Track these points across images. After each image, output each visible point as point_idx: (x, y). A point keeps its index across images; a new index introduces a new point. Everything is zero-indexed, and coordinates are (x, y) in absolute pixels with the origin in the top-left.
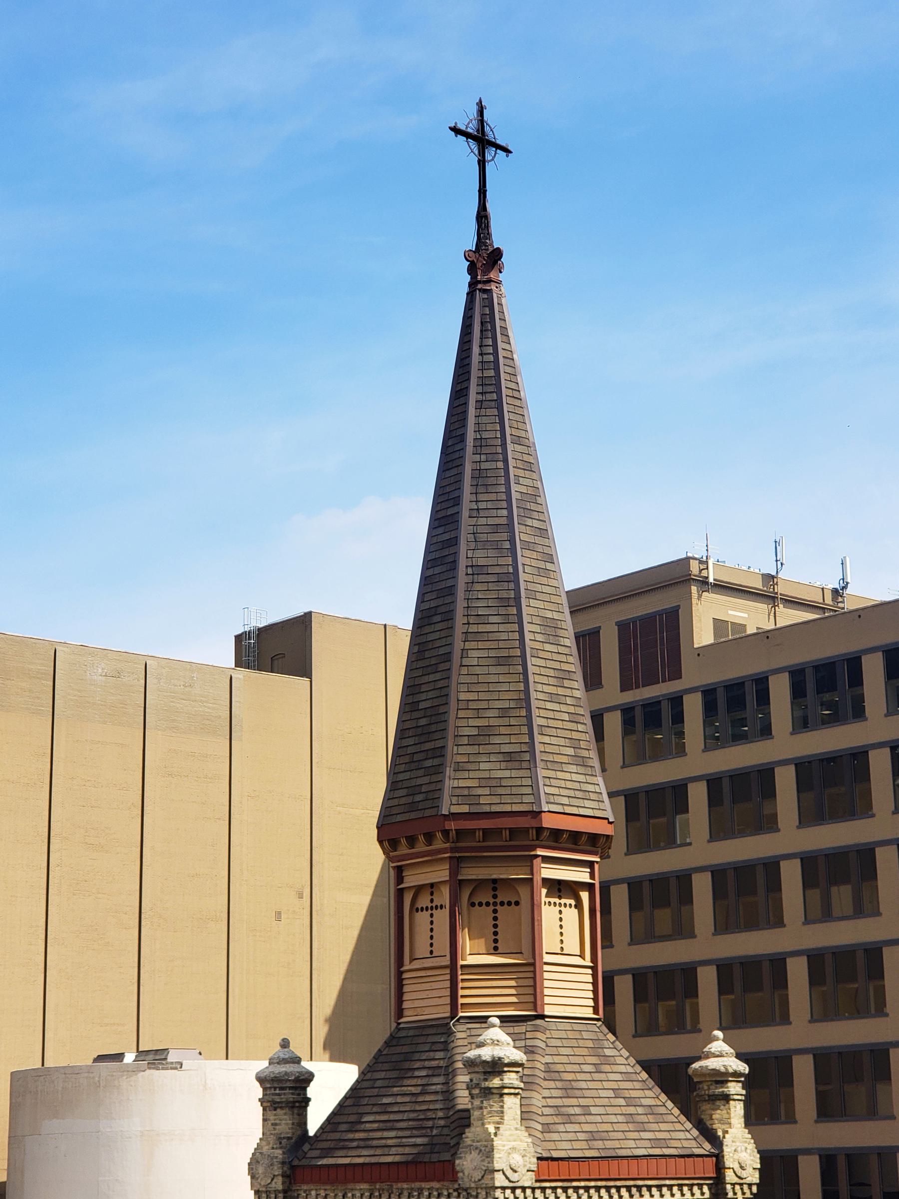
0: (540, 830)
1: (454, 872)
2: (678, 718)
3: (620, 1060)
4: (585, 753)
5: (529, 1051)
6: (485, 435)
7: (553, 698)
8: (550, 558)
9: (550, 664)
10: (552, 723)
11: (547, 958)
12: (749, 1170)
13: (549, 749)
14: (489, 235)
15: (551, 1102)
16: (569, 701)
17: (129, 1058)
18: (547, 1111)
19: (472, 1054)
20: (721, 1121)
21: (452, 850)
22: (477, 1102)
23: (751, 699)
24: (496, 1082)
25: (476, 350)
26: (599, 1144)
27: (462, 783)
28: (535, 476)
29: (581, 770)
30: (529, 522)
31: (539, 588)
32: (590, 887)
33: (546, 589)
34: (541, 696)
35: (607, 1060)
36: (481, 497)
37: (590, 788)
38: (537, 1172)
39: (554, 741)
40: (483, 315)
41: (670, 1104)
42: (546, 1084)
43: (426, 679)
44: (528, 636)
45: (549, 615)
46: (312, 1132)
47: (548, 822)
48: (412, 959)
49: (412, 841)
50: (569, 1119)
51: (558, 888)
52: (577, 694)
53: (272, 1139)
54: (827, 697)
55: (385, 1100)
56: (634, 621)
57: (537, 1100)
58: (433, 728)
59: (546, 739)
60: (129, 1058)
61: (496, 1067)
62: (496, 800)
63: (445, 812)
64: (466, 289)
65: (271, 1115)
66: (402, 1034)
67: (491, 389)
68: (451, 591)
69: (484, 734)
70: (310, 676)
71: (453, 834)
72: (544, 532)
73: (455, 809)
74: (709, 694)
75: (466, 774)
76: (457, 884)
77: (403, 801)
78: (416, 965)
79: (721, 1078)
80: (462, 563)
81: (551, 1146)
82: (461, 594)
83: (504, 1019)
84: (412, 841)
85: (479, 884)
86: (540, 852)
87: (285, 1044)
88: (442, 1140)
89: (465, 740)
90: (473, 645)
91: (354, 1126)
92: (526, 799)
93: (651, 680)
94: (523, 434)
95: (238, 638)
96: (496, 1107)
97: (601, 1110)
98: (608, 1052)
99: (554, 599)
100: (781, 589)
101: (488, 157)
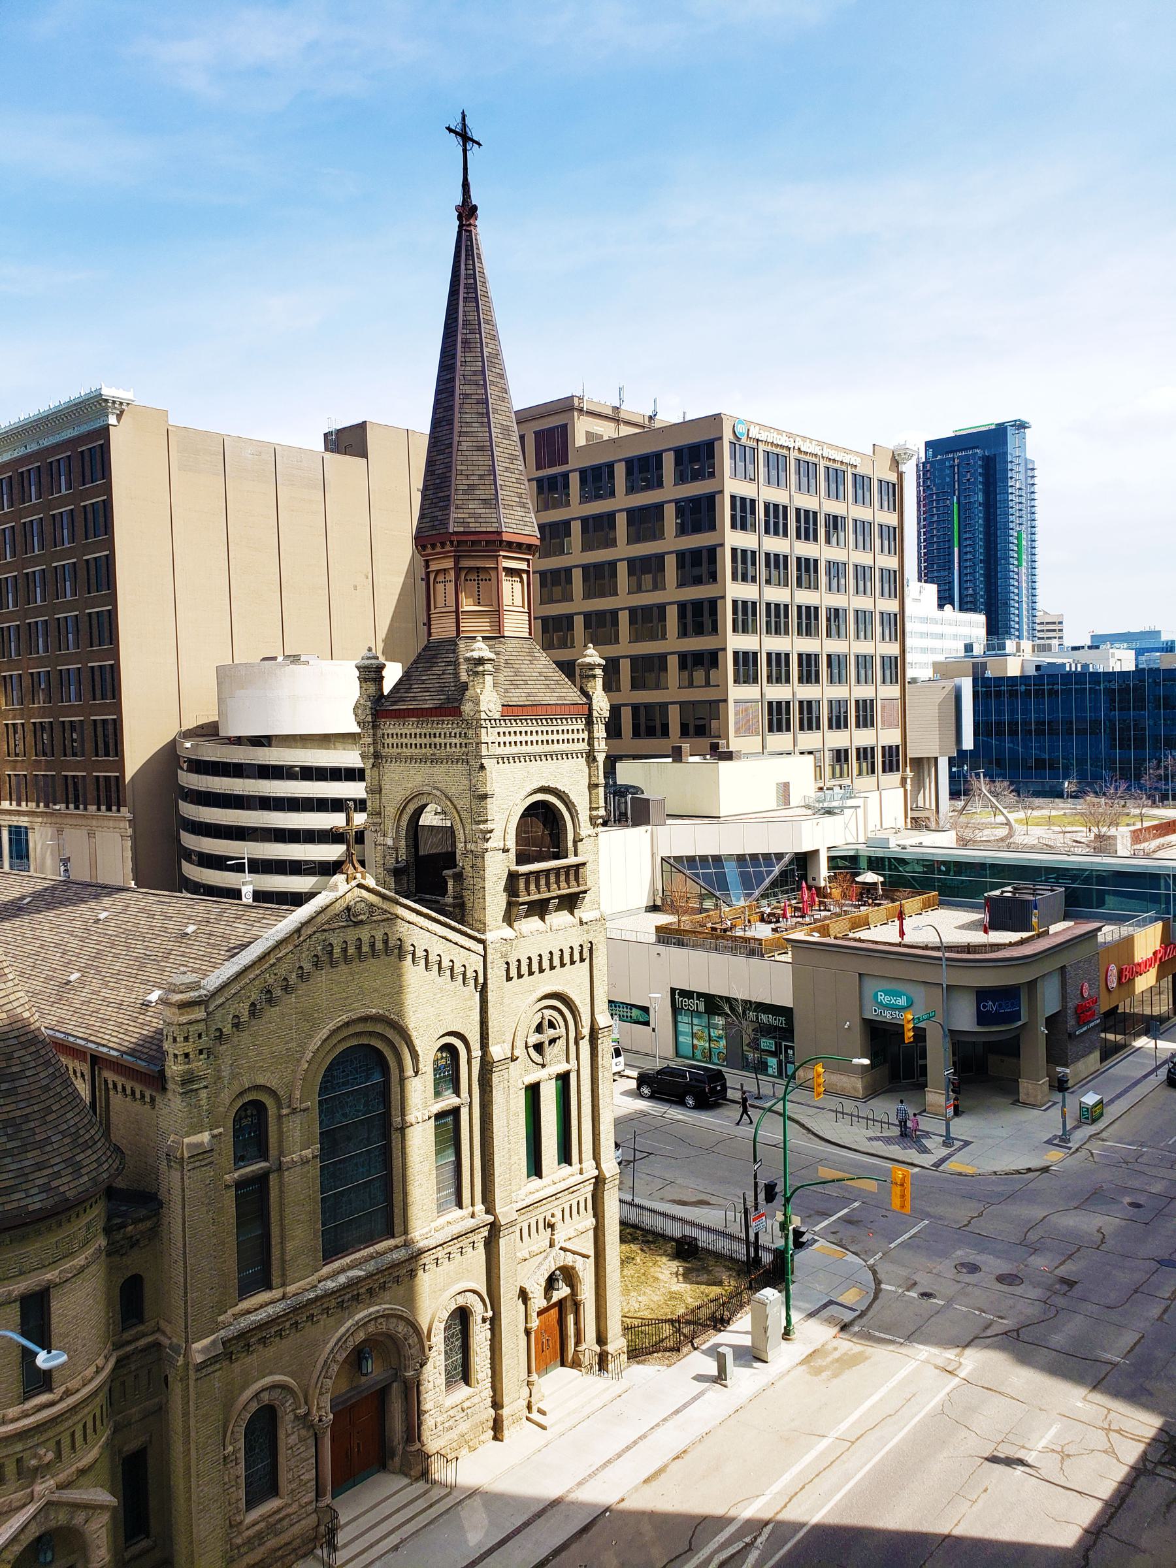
0: (501, 541)
1: (456, 563)
2: (566, 486)
3: (542, 658)
4: (525, 501)
5: (497, 653)
6: (469, 318)
7: (507, 470)
8: (505, 391)
9: (505, 451)
10: (507, 484)
11: (505, 608)
12: (605, 711)
13: (505, 498)
14: (470, 197)
15: (508, 678)
16: (516, 472)
17: (280, 659)
18: (506, 682)
19: (468, 655)
20: (591, 688)
21: (455, 551)
22: (471, 678)
23: (605, 477)
24: (481, 668)
25: (463, 267)
26: (532, 699)
27: (460, 516)
28: (497, 343)
29: (523, 509)
30: (494, 370)
31: (499, 407)
32: (527, 572)
33: (503, 408)
34: (501, 468)
35: (536, 658)
36: (467, 354)
37: (528, 519)
38: (502, 712)
39: (508, 493)
40: (467, 246)
41: (567, 680)
42: (505, 670)
43: (438, 457)
44: (494, 435)
45: (505, 423)
46: (386, 694)
47: (506, 537)
48: (435, 608)
49: (433, 546)
50: (517, 686)
51: (511, 572)
52: (520, 468)
53: (365, 696)
54: (644, 475)
55: (424, 678)
56: (543, 431)
57: (501, 678)
58: (443, 485)
59: (504, 493)
60: (280, 659)
61: (481, 661)
62: (478, 525)
63: (451, 531)
64: (457, 229)
65: (364, 685)
66: (431, 645)
67: (472, 290)
68: (451, 408)
69: (471, 489)
70: (364, 455)
71: (455, 543)
72: (502, 376)
73: (456, 530)
74: (583, 472)
75: (462, 511)
76: (458, 570)
77: (428, 525)
78: (437, 610)
79: (592, 667)
80: (457, 392)
81: (508, 699)
82: (457, 410)
83: (484, 638)
84: (433, 546)
85: (470, 570)
86: (502, 553)
87: (370, 650)
88: (454, 697)
89: (461, 492)
90: (464, 439)
91: (408, 690)
92: (494, 525)
93: (552, 464)
94: (490, 318)
95: (326, 435)
96: (481, 681)
97: (533, 682)
98: (536, 654)
99: (507, 414)
100: (622, 415)
101: (468, 148)
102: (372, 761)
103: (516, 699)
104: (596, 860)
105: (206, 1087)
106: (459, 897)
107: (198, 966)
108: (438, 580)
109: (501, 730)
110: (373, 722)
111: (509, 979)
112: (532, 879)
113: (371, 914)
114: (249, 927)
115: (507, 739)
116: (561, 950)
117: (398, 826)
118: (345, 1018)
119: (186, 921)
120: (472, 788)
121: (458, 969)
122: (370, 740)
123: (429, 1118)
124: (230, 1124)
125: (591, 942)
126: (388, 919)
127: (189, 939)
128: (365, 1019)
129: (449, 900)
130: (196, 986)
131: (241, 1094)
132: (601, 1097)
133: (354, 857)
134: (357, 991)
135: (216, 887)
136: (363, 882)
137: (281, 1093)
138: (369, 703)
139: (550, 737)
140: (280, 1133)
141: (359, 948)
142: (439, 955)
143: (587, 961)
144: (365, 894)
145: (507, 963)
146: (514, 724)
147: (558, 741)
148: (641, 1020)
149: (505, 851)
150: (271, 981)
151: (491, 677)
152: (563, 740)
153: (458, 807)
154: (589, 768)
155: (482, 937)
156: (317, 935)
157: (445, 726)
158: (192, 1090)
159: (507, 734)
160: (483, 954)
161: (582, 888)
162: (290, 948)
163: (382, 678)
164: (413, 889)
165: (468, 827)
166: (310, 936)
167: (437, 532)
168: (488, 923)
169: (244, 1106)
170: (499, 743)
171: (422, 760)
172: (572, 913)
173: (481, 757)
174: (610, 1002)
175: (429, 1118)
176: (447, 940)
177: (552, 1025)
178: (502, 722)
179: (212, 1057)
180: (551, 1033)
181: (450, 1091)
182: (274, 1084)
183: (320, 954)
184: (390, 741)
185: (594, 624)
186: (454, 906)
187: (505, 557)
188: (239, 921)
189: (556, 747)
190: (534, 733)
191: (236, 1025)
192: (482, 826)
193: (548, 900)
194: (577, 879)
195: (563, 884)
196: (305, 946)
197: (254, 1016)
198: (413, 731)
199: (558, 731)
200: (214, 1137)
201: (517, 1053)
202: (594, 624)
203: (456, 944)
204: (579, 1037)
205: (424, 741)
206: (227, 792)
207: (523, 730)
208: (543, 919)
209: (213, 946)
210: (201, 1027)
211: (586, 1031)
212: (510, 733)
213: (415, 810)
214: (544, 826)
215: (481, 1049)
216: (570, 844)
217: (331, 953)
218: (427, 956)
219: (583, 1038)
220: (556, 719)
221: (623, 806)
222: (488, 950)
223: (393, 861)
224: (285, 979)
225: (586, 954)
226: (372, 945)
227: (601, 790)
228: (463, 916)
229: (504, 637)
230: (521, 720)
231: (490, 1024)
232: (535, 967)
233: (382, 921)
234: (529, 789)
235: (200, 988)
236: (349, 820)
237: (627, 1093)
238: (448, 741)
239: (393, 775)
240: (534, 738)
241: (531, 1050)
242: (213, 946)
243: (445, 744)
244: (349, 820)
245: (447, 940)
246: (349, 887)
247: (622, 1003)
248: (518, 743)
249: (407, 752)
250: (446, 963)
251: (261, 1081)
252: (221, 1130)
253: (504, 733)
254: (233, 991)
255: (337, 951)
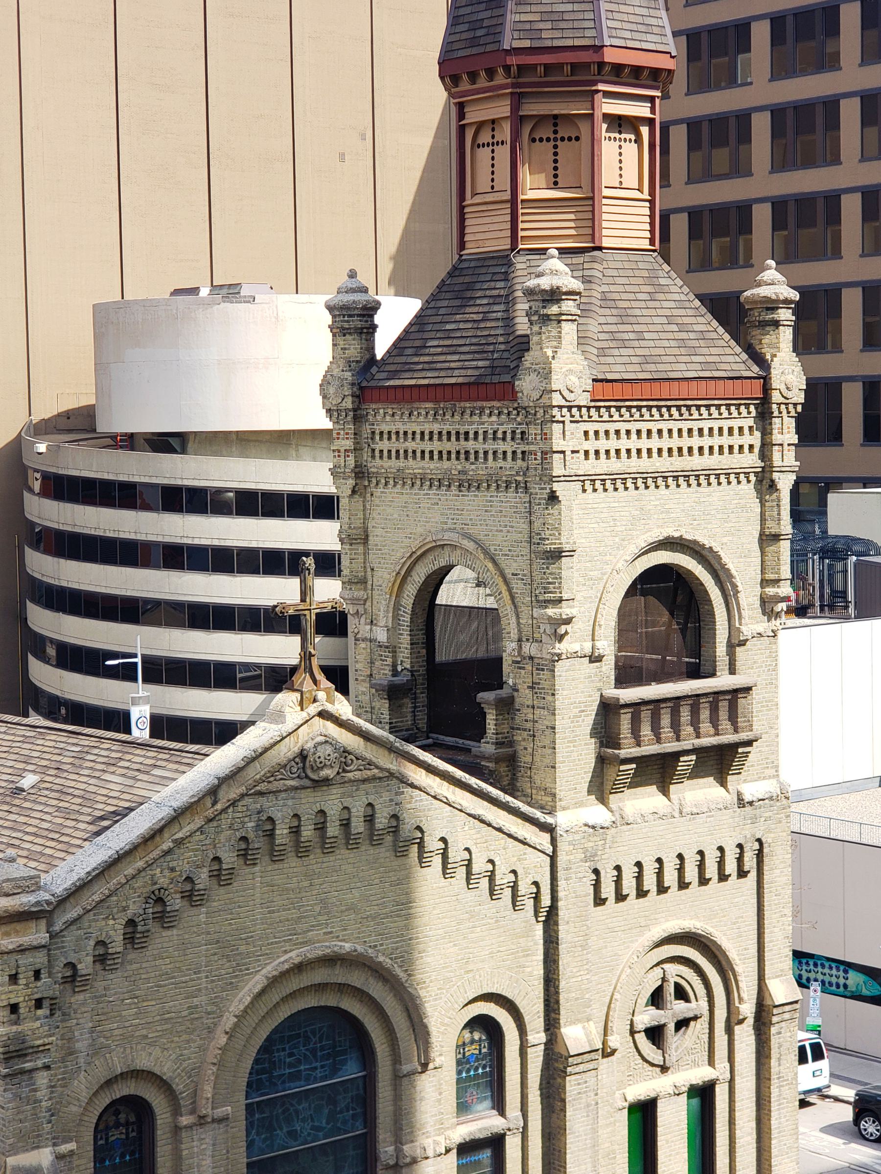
0: (601, 64)
1: (515, 108)
5: (586, 280)
11: (606, 192)
15: (606, 328)
17: (204, 292)
18: (602, 336)
19: (532, 283)
20: (770, 346)
21: (514, 85)
22: (536, 328)
24: (554, 309)
26: (652, 367)
27: (524, 17)
32: (650, 122)
35: (662, 289)
41: (721, 330)
47: (610, 56)
48: (474, 194)
49: (473, 77)
50: (624, 344)
51: (619, 123)
53: (342, 363)
55: (448, 327)
57: (593, 326)
60: (204, 292)
61: (554, 296)
62: (558, 34)
63: (506, 47)
65: (341, 341)
71: (514, 70)
73: (516, 44)
76: (518, 120)
77: (464, 36)
79: (771, 305)
81: (606, 368)
84: (473, 77)
85: (540, 120)
86: (601, 87)
91: (419, 350)
92: (589, 33)
96: (554, 333)
98: (662, 281)
102: (351, 482)
103: (621, 368)
104: (773, 684)
105: (47, 1067)
106: (506, 742)
107: (38, 849)
108: (480, 141)
109: (591, 427)
110: (355, 410)
111: (599, 901)
112: (646, 715)
113: (344, 768)
114: (130, 782)
115: (603, 444)
116: (701, 853)
117: (397, 607)
118: (295, 956)
119: (22, 766)
120: (534, 539)
121: (503, 878)
122: (348, 444)
123: (448, 1151)
124: (88, 1136)
125: (759, 841)
126: (374, 778)
127: (25, 799)
128: (331, 960)
129: (487, 747)
130: (32, 884)
131: (109, 1083)
132: (774, 1134)
133: (315, 662)
134: (317, 909)
135: (87, 705)
136: (329, 707)
137: (179, 1086)
138: (348, 375)
139: (685, 442)
140: (177, 1156)
141: (321, 828)
142: (467, 849)
143: (753, 875)
144: (332, 729)
145: (596, 872)
146: (616, 417)
147: (701, 449)
148: (865, 992)
149: (595, 659)
150: (163, 881)
151: (574, 326)
152: (711, 448)
153: (508, 572)
154: (762, 503)
155: (549, 820)
156: (247, 801)
157: (485, 418)
158: (23, 1072)
159: (602, 434)
160: (549, 850)
161: (743, 736)
162: (199, 822)
163: (374, 327)
164: (423, 724)
165: (525, 611)
166: (234, 803)
167: (481, 50)
168: (560, 794)
169: (114, 1106)
170: (586, 453)
171: (441, 483)
172: (723, 783)
173: (552, 479)
174: (798, 955)
175: (448, 1151)
176: (483, 821)
177: (681, 994)
178: (593, 411)
179: (58, 1013)
180: (680, 1008)
181: (488, 1103)
182: (166, 1069)
183: (251, 835)
184: (385, 445)
185: (792, 221)
186: (497, 760)
187: (607, 94)
188: (112, 769)
189: (696, 462)
190: (655, 434)
191: (102, 959)
192: (551, 611)
193: (676, 756)
194: (733, 717)
195: (706, 726)
196: (225, 821)
197: (133, 943)
198: (427, 428)
199: (701, 431)
200: (60, 1157)
201: (614, 1041)
202: (792, 221)
203: (499, 830)
204: (734, 1020)
205: (446, 446)
206: (108, 534)
207: (633, 427)
208: (665, 791)
209: (67, 813)
210: (40, 959)
211: (747, 1009)
212: (607, 433)
213: (429, 577)
214: (672, 614)
215: (546, 1030)
216: (721, 650)
217: (271, 835)
218: (446, 849)
219: (741, 1022)
220: (698, 407)
221: (839, 577)
222: (560, 845)
223: (388, 671)
224: (189, 879)
225: (750, 862)
226: (346, 825)
227: (785, 547)
228: (514, 779)
229: (600, 248)
230: (629, 408)
231: (563, 984)
232: (650, 882)
233: (364, 781)
234: (643, 541)
235: (39, 888)
236: (305, 592)
237: (833, 1129)
238: (490, 446)
239: (389, 510)
240: (655, 443)
241: (641, 1038)
242: (67, 813)
243: (486, 453)
244: (305, 592)
245: (483, 821)
246: (304, 715)
247: (828, 959)
248: (623, 453)
249: (415, 466)
250: (480, 866)
251: (143, 1062)
252: (72, 1146)
253: (596, 433)
254: (96, 898)
255: (282, 832)
